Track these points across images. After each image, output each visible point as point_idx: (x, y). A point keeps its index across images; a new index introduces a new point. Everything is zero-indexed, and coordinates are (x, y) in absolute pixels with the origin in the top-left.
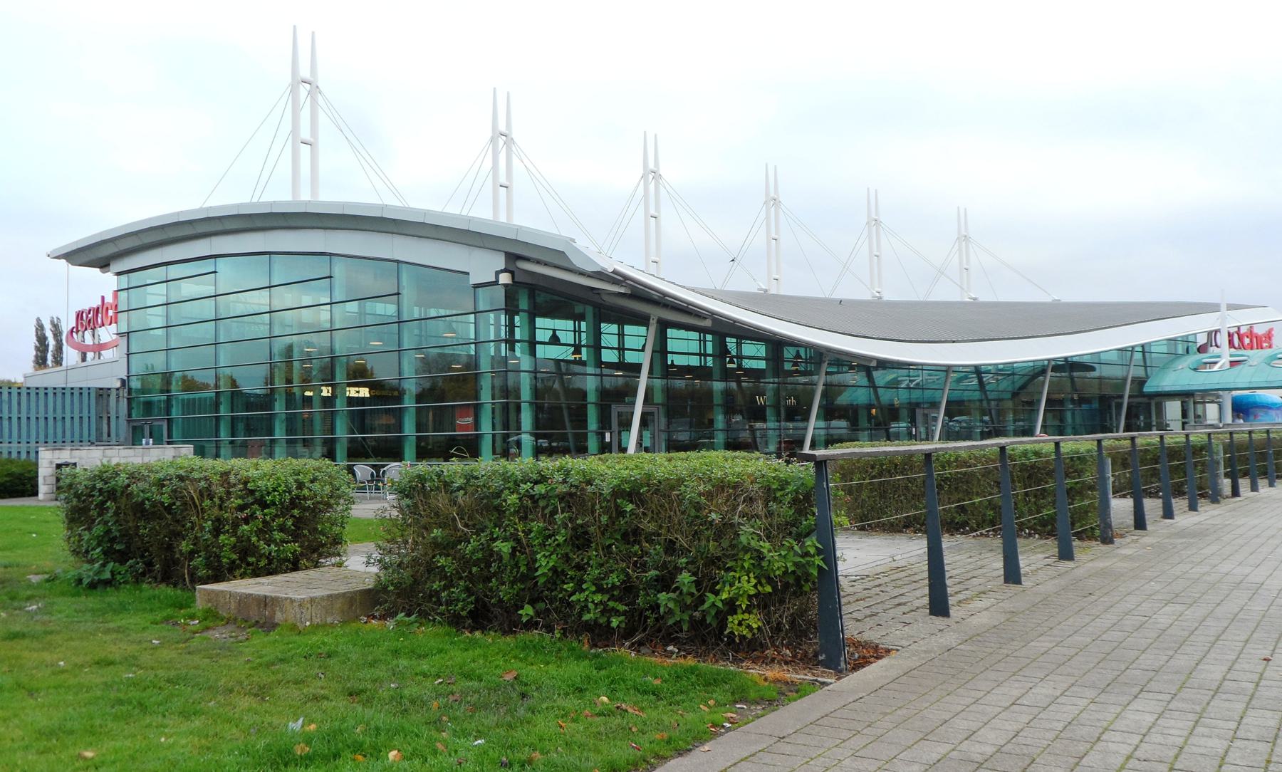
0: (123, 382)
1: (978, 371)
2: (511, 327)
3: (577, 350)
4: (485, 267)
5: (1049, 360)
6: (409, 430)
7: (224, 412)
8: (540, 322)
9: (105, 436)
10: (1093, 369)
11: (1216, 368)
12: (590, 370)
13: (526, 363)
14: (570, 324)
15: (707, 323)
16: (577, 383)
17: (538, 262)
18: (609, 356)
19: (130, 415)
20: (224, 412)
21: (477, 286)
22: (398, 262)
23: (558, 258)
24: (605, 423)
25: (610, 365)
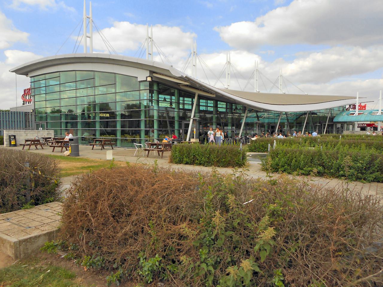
0: (33, 110)
1: (286, 113)
2: (152, 97)
3: (171, 104)
4: (143, 76)
5: (308, 111)
6: (119, 128)
7: (63, 120)
8: (160, 96)
9: (28, 126)
10: (316, 114)
11: (354, 115)
12: (176, 110)
13: (156, 107)
14: (169, 97)
15: (214, 96)
16: (171, 115)
17: (160, 74)
18: (181, 107)
19: (35, 120)
20: (63, 120)
21: (140, 82)
22: (115, 73)
23: (166, 72)
24: (180, 126)
25: (181, 109)
